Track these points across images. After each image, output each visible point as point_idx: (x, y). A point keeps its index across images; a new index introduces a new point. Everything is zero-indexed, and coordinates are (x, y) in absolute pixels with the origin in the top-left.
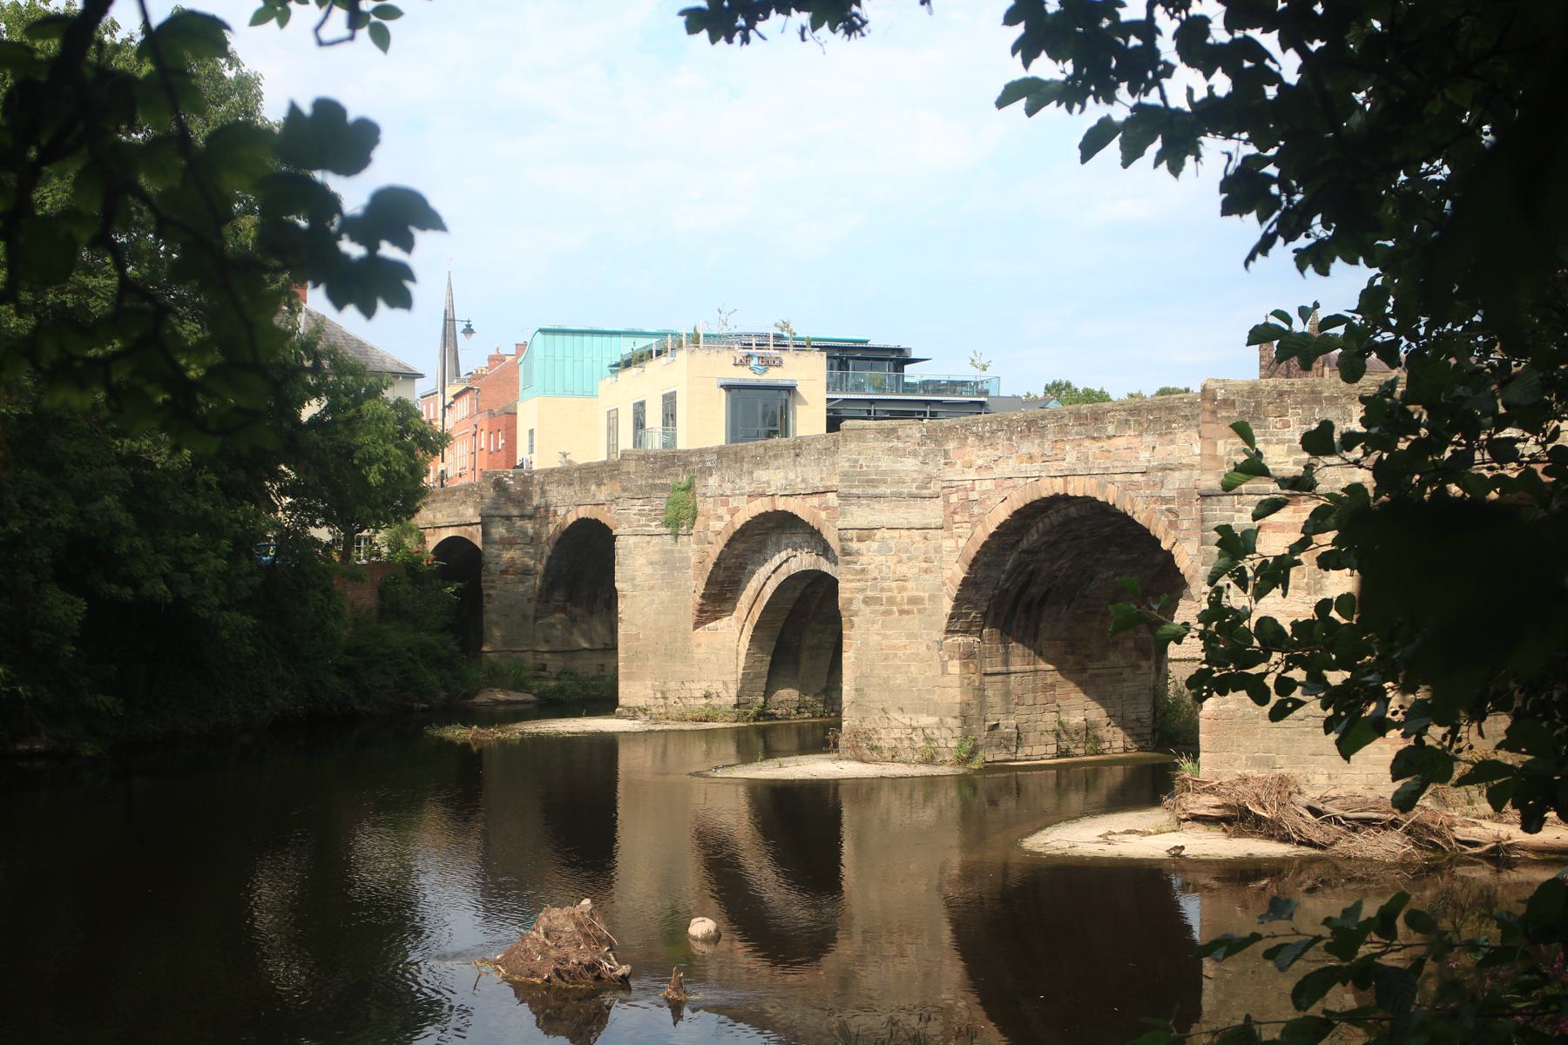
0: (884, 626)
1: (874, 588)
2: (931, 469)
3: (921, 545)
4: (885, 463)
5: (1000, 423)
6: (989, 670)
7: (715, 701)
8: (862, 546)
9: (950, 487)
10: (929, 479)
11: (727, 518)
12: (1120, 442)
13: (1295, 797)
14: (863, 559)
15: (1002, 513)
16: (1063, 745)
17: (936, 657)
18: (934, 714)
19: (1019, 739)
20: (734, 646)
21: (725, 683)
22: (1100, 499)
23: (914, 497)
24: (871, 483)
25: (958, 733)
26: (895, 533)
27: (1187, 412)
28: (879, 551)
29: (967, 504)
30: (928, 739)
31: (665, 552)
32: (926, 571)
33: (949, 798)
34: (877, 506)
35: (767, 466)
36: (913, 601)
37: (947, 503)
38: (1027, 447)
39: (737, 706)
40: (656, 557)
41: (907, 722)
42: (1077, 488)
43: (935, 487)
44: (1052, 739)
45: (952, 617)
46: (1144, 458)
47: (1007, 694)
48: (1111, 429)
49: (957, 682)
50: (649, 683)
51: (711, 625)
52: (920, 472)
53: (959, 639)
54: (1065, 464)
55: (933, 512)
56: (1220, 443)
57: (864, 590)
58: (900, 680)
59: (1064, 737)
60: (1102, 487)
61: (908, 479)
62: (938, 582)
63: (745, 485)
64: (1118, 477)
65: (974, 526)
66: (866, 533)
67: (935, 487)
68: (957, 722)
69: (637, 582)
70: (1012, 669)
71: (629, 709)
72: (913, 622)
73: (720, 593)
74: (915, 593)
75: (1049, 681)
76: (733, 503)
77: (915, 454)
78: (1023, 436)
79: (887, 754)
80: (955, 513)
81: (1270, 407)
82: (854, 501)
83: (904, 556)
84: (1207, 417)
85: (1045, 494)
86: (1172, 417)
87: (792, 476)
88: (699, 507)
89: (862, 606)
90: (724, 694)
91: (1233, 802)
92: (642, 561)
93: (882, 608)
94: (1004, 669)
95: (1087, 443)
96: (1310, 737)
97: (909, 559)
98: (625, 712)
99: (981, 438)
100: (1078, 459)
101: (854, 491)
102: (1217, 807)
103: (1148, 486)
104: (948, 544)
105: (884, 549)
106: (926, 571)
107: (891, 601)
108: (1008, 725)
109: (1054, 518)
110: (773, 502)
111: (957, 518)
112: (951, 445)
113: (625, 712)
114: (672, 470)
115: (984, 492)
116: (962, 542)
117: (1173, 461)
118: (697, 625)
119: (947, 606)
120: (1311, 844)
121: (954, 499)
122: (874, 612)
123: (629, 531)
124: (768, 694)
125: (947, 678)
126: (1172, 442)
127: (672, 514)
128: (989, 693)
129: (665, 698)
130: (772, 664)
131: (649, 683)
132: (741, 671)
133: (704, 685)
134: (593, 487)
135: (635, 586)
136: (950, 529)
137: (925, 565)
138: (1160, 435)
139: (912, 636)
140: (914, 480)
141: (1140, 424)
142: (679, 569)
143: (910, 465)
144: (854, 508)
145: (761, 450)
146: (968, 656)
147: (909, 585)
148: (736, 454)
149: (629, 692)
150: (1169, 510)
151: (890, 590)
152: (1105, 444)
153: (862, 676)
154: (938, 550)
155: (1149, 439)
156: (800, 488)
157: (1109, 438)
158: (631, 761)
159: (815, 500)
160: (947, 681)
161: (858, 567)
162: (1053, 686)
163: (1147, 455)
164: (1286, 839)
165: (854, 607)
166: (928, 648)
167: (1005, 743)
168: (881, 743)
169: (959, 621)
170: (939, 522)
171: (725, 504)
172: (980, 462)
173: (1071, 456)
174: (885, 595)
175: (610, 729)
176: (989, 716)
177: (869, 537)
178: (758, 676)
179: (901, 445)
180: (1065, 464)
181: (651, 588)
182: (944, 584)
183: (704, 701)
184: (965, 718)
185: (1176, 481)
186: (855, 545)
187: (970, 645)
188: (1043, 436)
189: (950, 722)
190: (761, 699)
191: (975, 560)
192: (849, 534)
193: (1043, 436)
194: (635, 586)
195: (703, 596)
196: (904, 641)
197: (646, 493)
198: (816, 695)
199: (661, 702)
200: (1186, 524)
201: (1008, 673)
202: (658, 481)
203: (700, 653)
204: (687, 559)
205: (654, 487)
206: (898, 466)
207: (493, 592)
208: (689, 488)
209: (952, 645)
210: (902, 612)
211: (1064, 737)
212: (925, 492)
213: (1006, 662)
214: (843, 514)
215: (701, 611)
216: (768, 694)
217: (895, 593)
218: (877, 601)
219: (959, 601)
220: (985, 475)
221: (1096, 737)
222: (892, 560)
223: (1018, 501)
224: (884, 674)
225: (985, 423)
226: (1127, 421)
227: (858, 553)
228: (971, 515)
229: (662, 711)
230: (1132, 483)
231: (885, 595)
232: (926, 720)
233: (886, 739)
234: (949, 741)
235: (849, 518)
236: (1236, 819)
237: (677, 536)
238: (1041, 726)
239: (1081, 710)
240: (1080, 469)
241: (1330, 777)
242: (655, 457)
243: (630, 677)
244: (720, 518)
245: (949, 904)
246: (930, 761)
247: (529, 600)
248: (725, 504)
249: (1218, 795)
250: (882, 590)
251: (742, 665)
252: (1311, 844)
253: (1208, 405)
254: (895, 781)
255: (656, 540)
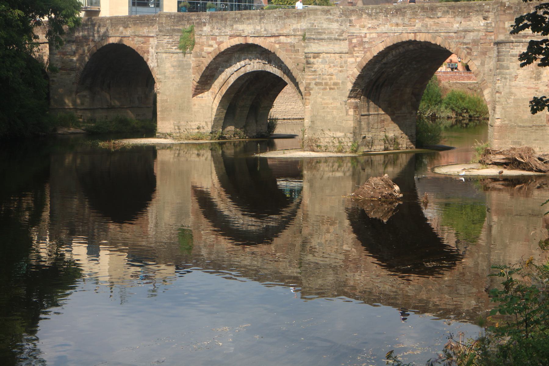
0: (323, 95)
1: (319, 78)
2: (343, 27)
3: (339, 60)
4: (325, 25)
5: (381, 9)
6: (363, 114)
7: (202, 131)
8: (315, 60)
9: (352, 35)
10: (343, 32)
11: (216, 46)
12: (445, 20)
13: (533, 154)
14: (315, 66)
15: (381, 47)
16: (387, 145)
17: (344, 108)
18: (342, 132)
19: (372, 143)
20: (210, 105)
21: (206, 122)
22: (433, 42)
23: (336, 39)
24: (320, 34)
25: (352, 140)
26: (329, 55)
27: (478, 8)
28: (322, 63)
29: (361, 43)
30: (340, 142)
31: (179, 61)
32: (341, 71)
33: (348, 166)
34: (321, 43)
35: (242, 23)
36: (335, 84)
37: (350, 42)
38: (394, 20)
39: (211, 133)
40: (175, 64)
41: (332, 135)
42: (421, 38)
43: (345, 36)
44: (382, 143)
45: (351, 91)
46: (456, 26)
47: (368, 124)
48: (439, 14)
49: (352, 118)
50: (172, 122)
51: (200, 95)
52: (339, 29)
53: (353, 100)
54: (415, 28)
55: (344, 46)
56: (506, 23)
57: (315, 79)
58: (329, 117)
59: (387, 142)
60: (435, 38)
61: (334, 32)
62: (346, 76)
63: (229, 31)
64: (442, 34)
65: (365, 52)
66: (317, 55)
67: (345, 36)
68: (352, 135)
69: (167, 75)
70: (371, 113)
71: (163, 134)
72: (335, 93)
73: (205, 81)
74: (336, 81)
75: (382, 118)
76: (219, 39)
77: (337, 21)
78: (393, 15)
79: (323, 149)
80: (355, 47)
81: (525, 9)
82: (312, 41)
83: (332, 65)
84: (502, 13)
85: (404, 40)
86: (470, 11)
87: (258, 28)
88: (197, 40)
89: (314, 86)
90: (206, 127)
91: (510, 157)
92: (168, 65)
93: (322, 87)
94: (366, 113)
95: (427, 19)
96: (533, 134)
97: (334, 66)
98: (161, 136)
99: (370, 15)
100: (422, 26)
101: (312, 37)
102: (504, 159)
103: (457, 38)
104: (351, 60)
105: (324, 62)
106: (341, 71)
107: (326, 84)
108: (369, 136)
109: (401, 50)
110: (246, 39)
111: (356, 49)
112: (353, 18)
113: (161, 136)
114: (182, 22)
115: (371, 38)
116: (359, 60)
117: (470, 28)
118: (195, 95)
119: (350, 86)
120: (540, 171)
121: (355, 41)
122: (319, 89)
123: (163, 51)
124: (223, 128)
125: (348, 117)
126: (470, 20)
127: (182, 43)
128: (363, 123)
129: (179, 129)
130: (227, 113)
131: (172, 122)
132: (214, 117)
133: (197, 123)
134: (121, 28)
135: (165, 77)
136: (352, 53)
137: (340, 69)
138: (464, 17)
139: (334, 99)
140: (337, 33)
141: (454, 13)
142: (185, 69)
143: (335, 26)
144: (312, 44)
145: (239, 16)
146: (356, 107)
147: (334, 77)
148: (222, 16)
149: (162, 126)
150: (467, 48)
151: (326, 79)
152: (436, 20)
153: (314, 116)
154: (346, 62)
155: (459, 19)
156: (264, 33)
157: (438, 18)
158: (162, 156)
159: (273, 40)
160: (349, 118)
161: (313, 69)
162: (383, 121)
163: (458, 25)
164: (531, 170)
165: (311, 86)
166: (341, 104)
167: (367, 145)
168: (321, 144)
169: (354, 93)
170: (346, 50)
171: (215, 39)
172: (370, 26)
173: (418, 25)
174: (324, 82)
175: (165, 143)
176: (363, 133)
177: (318, 57)
178: (220, 119)
179: (331, 17)
180: (415, 28)
181: (173, 78)
182: (348, 77)
183: (197, 131)
184: (354, 133)
185: (470, 37)
186: (312, 60)
187: (356, 103)
188: (404, 16)
189: (349, 135)
190: (221, 130)
191: (365, 67)
192: (310, 55)
193: (404, 16)
194: (165, 77)
195: (198, 82)
196: (331, 101)
197: (171, 33)
198: (241, 128)
199: (178, 131)
200: (475, 53)
201: (369, 115)
202: (176, 28)
203: (195, 108)
204: (190, 64)
205: (174, 30)
206: (330, 26)
207: (55, 79)
208: (191, 31)
209: (351, 103)
210: (330, 89)
211: (387, 142)
212: (341, 38)
213: (368, 111)
214: (308, 46)
215: (196, 89)
216: (223, 128)
217: (328, 81)
218: (320, 84)
219: (355, 84)
220: (372, 31)
221: (397, 143)
222: (327, 66)
223: (389, 43)
224: (323, 115)
225: (372, 9)
226: (448, 11)
227: (313, 63)
228: (364, 48)
229: (178, 135)
230: (449, 37)
231: (324, 82)
232: (339, 134)
233: (323, 142)
234: (348, 143)
235: (310, 48)
236: (511, 163)
237: (184, 53)
238: (379, 138)
239: (393, 131)
240: (423, 30)
241: (540, 148)
242: (174, 16)
243: (163, 119)
244: (212, 46)
245: (347, 209)
246: (340, 151)
247: (73, 83)
248: (215, 39)
249: (504, 155)
250: (323, 79)
251: (214, 114)
252: (540, 171)
253: (503, 8)
254: (326, 160)
255: (175, 55)
